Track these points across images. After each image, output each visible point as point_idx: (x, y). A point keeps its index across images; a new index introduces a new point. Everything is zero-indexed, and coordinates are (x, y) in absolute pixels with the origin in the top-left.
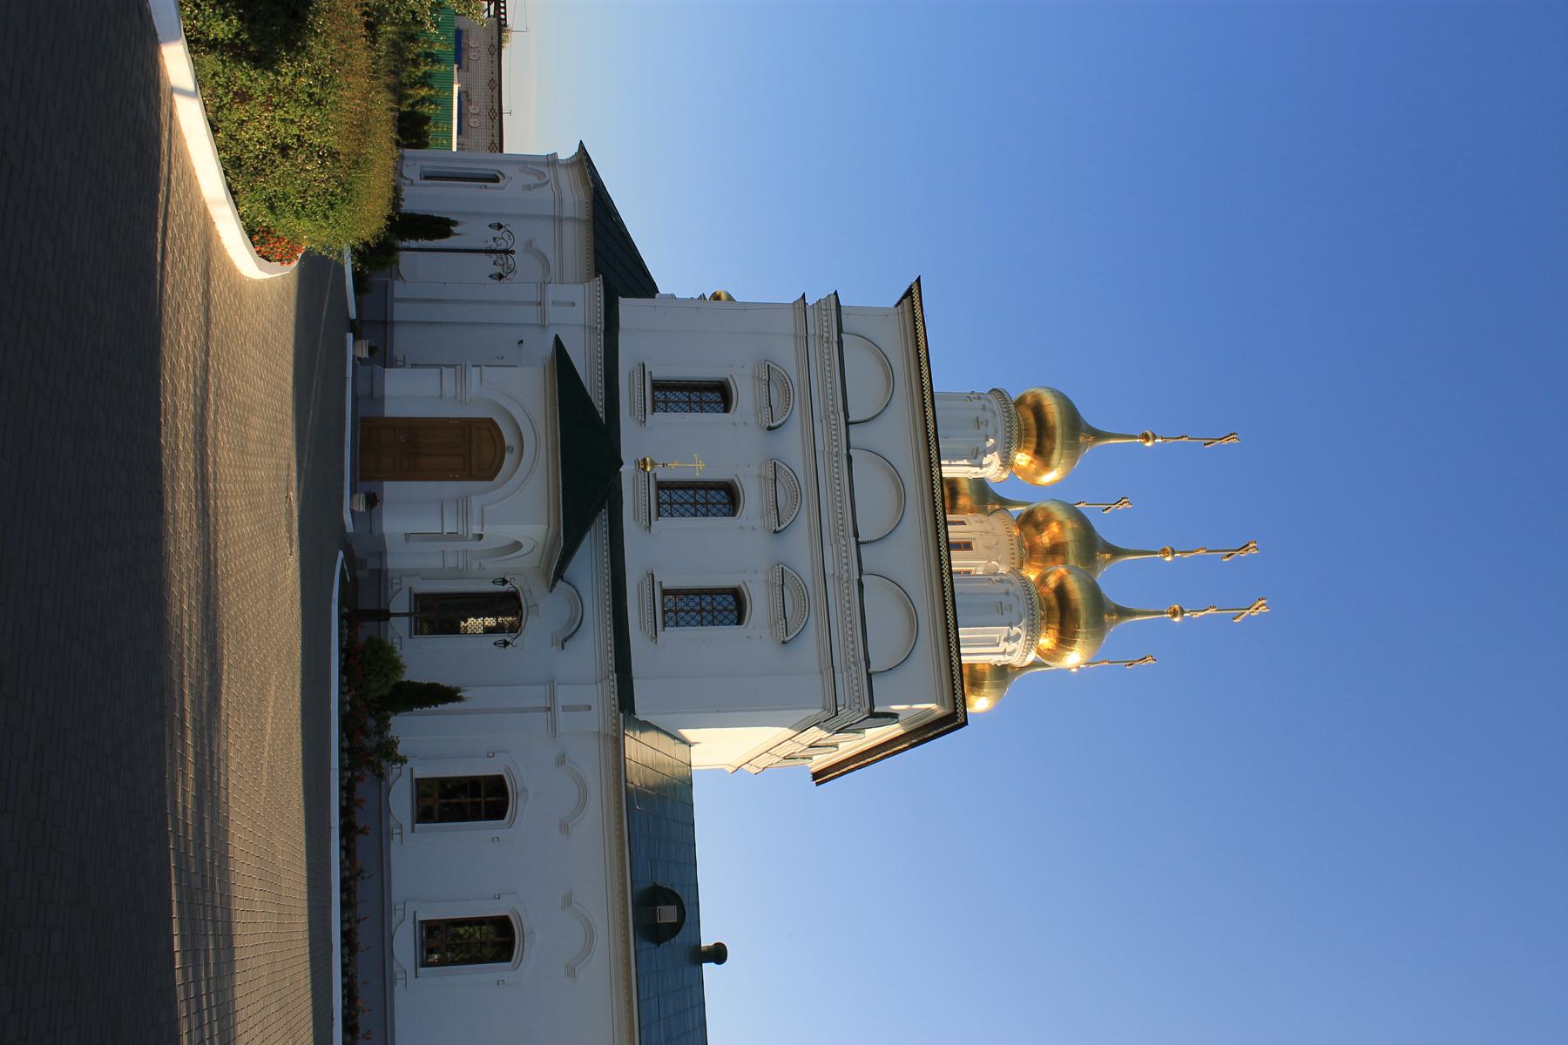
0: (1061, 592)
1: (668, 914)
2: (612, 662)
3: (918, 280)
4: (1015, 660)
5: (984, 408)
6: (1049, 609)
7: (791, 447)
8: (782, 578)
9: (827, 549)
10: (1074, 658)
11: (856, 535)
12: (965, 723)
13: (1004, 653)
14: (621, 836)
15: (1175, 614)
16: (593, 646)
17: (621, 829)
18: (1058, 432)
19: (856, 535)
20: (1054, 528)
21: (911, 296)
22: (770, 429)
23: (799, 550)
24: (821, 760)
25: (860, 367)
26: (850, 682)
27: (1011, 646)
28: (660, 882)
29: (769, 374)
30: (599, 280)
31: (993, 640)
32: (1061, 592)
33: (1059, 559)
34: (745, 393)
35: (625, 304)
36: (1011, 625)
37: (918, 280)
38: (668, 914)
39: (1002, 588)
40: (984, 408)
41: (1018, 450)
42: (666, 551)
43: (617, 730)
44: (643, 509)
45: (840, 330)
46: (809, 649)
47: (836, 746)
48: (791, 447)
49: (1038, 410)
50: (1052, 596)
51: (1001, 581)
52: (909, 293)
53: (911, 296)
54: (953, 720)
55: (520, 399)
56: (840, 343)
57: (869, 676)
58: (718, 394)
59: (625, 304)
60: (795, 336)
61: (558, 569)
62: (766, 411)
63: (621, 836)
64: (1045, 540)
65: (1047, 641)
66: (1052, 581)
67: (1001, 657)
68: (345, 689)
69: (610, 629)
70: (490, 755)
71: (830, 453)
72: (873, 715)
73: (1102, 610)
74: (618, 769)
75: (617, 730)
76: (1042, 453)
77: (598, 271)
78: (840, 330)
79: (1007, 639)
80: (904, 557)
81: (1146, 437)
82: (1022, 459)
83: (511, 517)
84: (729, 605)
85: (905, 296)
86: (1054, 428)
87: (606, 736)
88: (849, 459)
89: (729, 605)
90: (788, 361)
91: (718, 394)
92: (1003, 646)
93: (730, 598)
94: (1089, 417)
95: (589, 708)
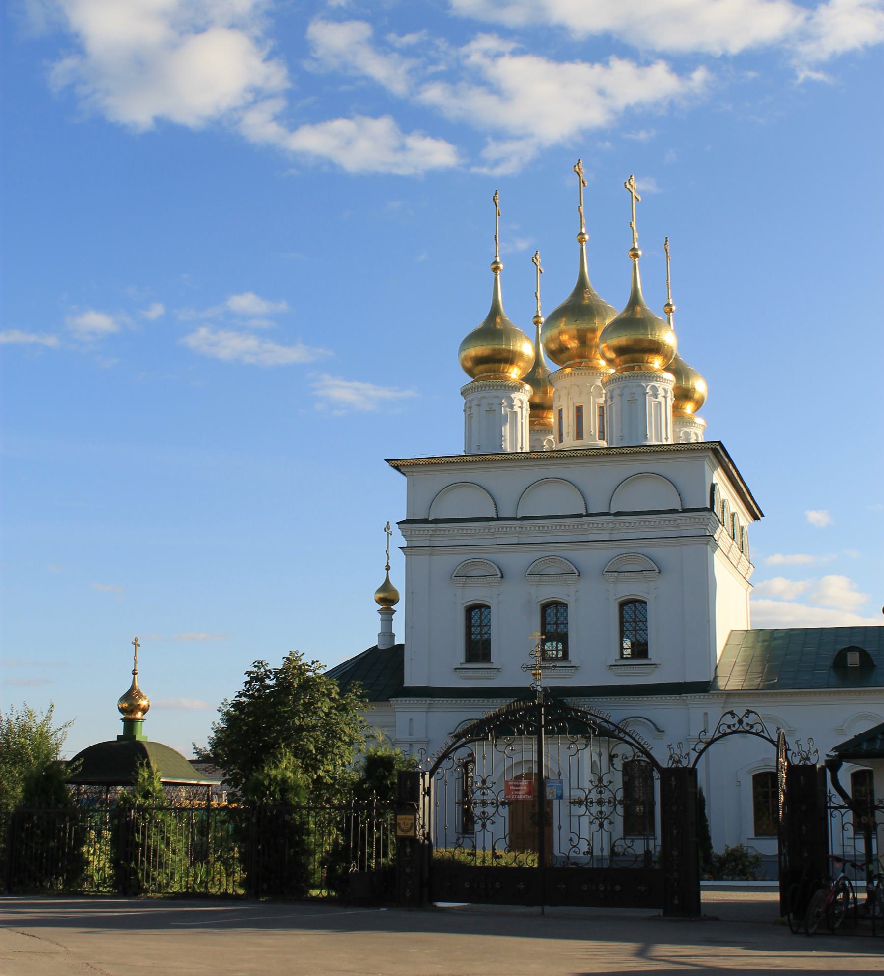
0: (621, 351)
1: (853, 659)
2: (673, 697)
3: (387, 461)
4: (670, 387)
5: (479, 405)
6: (633, 361)
7: (515, 561)
8: (613, 571)
9: (591, 538)
10: (668, 337)
11: (580, 516)
12: (720, 443)
13: (665, 397)
14: (796, 694)
15: (636, 255)
16: (664, 711)
17: (792, 694)
18: (496, 347)
19: (580, 516)
20: (565, 337)
21: (398, 465)
22: (502, 577)
23: (592, 558)
24: (744, 519)
25: (450, 507)
26: (687, 524)
27: (661, 392)
28: (829, 662)
29: (462, 576)
30: (393, 701)
31: (656, 406)
32: (621, 351)
33: (590, 335)
34: (476, 594)
35: (411, 680)
36: (645, 394)
37: (387, 461)
38: (853, 659)
39: (617, 399)
40: (479, 405)
41: (507, 378)
42: (596, 653)
43: (722, 695)
44: (564, 672)
45: (426, 521)
46: (663, 553)
47: (733, 515)
48: (515, 561)
49: (480, 361)
50: (623, 358)
51: (612, 398)
52: (397, 468)
53: (398, 465)
54: (718, 452)
55: (498, 764)
56: (436, 521)
57: (685, 511)
58: (476, 614)
59: (411, 680)
60: (430, 555)
61: (609, 733)
62: (489, 579)
63: (796, 694)
64: (573, 344)
65: (656, 362)
66: (611, 355)
67: (669, 399)
68: (744, 877)
69: (654, 698)
70: (739, 784)
71: (519, 533)
72: (712, 509)
73: (634, 319)
74: (749, 695)
75: (722, 695)
76: (510, 358)
77: (387, 700)
78: (426, 521)
79: (655, 395)
80: (598, 482)
81: (496, 270)
82: (514, 373)
83: (576, 766)
84: (632, 613)
85: (399, 470)
86: (494, 350)
87: (725, 703)
88: (524, 518)
89: (632, 613)
90: (448, 562)
91: (476, 614)
92: (660, 399)
93: (626, 608)
94: (478, 321)
95: (706, 713)
